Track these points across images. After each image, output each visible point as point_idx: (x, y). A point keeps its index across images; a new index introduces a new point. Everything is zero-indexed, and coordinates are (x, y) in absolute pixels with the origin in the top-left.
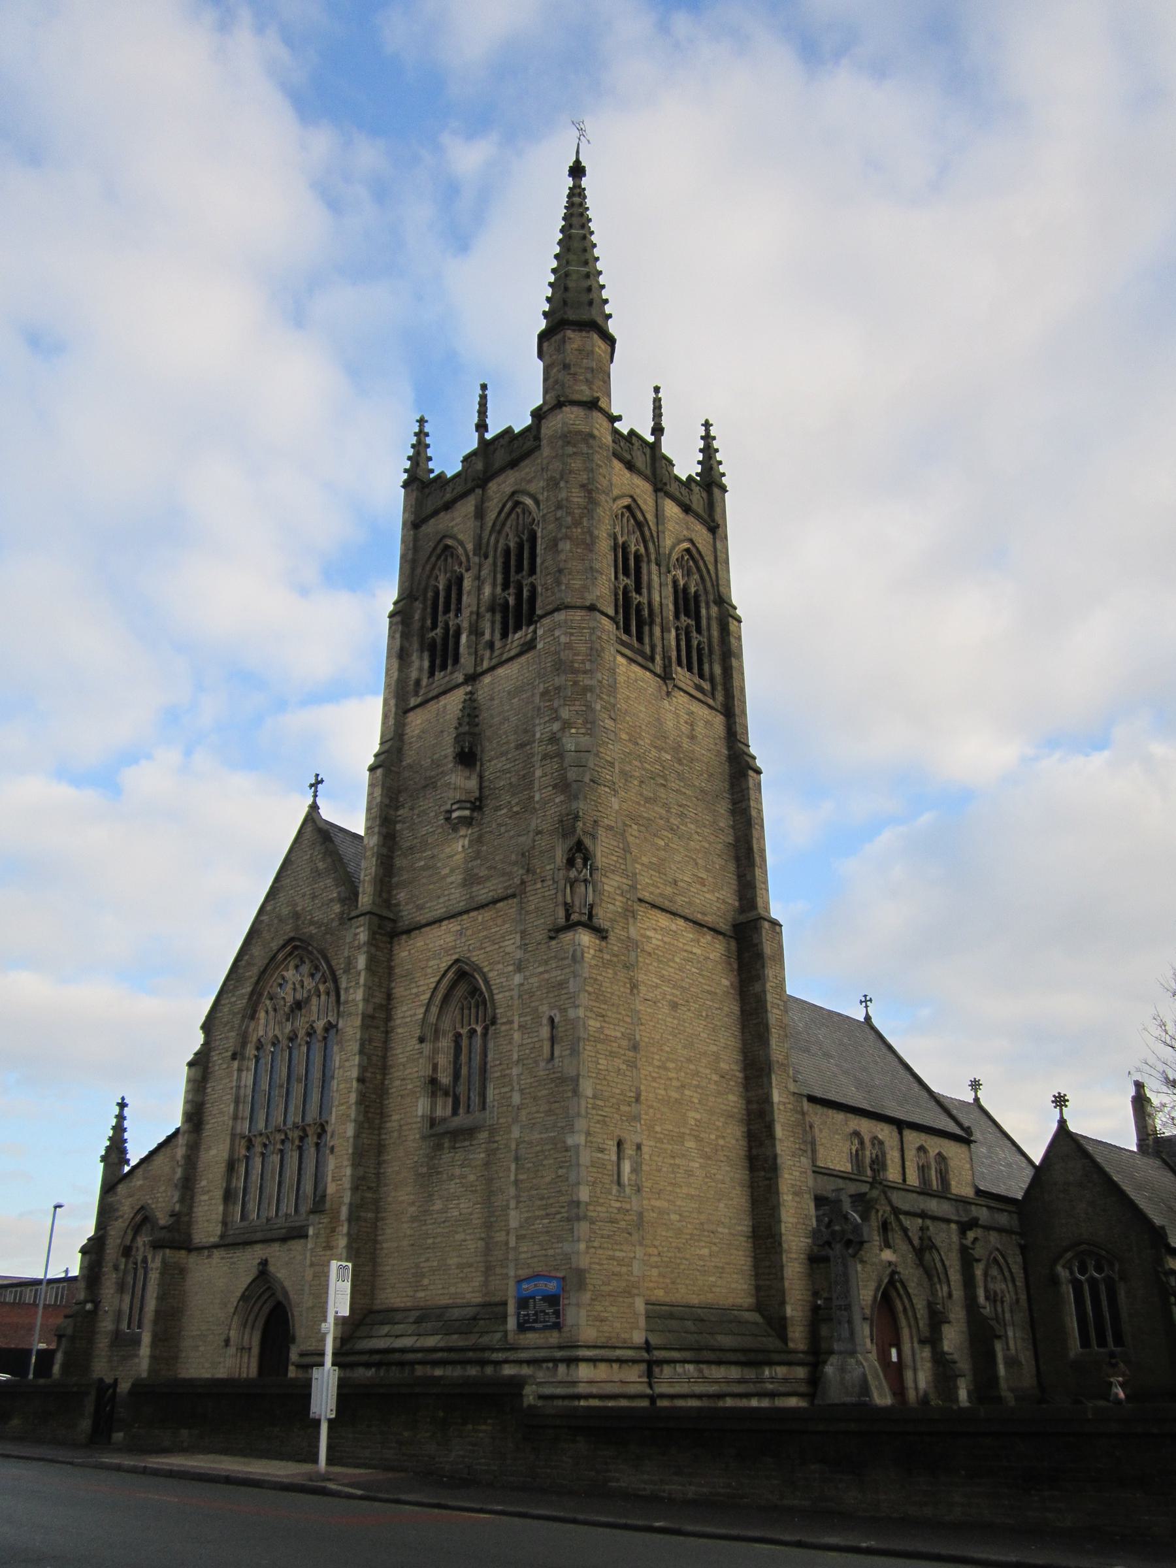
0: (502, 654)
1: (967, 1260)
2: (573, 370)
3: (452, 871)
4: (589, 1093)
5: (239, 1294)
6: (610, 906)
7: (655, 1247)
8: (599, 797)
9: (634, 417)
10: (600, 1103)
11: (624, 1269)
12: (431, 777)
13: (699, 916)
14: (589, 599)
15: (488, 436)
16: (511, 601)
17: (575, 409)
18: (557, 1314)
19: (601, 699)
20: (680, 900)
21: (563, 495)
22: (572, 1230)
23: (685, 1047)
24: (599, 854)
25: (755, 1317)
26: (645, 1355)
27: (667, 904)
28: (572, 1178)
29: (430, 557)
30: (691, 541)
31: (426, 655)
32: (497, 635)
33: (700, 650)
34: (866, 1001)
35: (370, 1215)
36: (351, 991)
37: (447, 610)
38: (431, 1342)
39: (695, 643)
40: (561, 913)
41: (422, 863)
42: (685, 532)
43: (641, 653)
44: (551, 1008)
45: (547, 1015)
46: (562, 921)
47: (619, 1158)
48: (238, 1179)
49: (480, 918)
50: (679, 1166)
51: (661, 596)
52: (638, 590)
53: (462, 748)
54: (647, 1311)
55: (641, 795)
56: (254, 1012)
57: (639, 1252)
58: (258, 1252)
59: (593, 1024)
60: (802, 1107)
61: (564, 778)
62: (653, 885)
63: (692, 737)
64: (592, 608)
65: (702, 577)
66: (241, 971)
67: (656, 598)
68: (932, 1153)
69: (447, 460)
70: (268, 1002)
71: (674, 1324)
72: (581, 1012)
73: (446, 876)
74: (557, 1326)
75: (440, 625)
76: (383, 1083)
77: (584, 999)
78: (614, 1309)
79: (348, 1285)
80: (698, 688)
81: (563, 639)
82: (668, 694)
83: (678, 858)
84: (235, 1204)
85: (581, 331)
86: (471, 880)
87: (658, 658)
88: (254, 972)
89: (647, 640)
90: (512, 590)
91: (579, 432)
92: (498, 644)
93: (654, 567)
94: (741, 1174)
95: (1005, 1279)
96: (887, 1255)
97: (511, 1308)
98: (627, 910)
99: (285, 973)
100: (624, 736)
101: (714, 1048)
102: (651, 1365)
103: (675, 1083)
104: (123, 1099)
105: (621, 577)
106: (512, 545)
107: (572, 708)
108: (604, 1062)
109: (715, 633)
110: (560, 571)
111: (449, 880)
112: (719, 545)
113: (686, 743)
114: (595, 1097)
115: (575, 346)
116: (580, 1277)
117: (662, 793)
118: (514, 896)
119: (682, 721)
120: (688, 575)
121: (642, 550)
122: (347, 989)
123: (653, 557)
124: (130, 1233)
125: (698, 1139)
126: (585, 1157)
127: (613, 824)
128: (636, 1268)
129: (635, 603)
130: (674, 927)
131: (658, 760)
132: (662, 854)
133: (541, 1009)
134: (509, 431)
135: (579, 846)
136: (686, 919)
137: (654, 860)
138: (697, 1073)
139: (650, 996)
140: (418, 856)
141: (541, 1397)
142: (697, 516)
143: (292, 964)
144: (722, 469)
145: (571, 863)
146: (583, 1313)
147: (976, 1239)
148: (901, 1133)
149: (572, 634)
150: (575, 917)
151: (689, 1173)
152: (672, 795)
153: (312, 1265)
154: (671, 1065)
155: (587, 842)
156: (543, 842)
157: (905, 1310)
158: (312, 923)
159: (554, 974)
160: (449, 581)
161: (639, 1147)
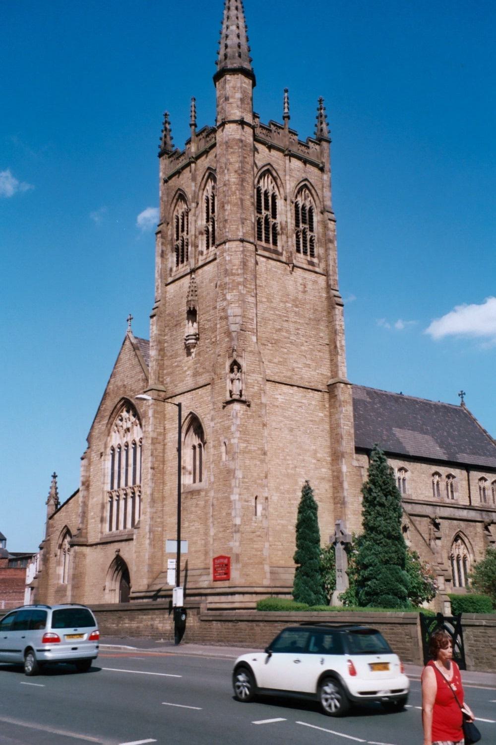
0: (206, 258)
2: (231, 100)
5: (109, 565)
6: (251, 389)
7: (280, 541)
8: (245, 337)
10: (246, 480)
11: (259, 553)
12: (178, 321)
13: (307, 383)
16: (211, 229)
19: (246, 287)
20: (295, 377)
21: (227, 178)
22: (233, 537)
29: (173, 200)
31: (175, 254)
34: (462, 394)
35: (160, 529)
36: (147, 426)
39: (308, 238)
40: (228, 394)
41: (176, 364)
45: (223, 441)
48: (107, 512)
49: (200, 393)
50: (293, 504)
51: (285, 216)
52: (274, 216)
53: (190, 308)
54: (270, 570)
55: (274, 328)
56: (109, 432)
58: (117, 546)
60: (361, 473)
61: (228, 329)
62: (280, 372)
63: (304, 292)
66: (102, 412)
70: (115, 427)
73: (186, 371)
76: (163, 468)
78: (254, 570)
80: (311, 263)
81: (228, 258)
84: (106, 523)
86: (196, 374)
87: (284, 253)
94: (332, 506)
98: (261, 390)
99: (122, 414)
100: (264, 300)
101: (314, 448)
103: (291, 466)
104: (55, 473)
105: (263, 211)
107: (232, 294)
108: (248, 462)
113: (300, 296)
114: (243, 478)
115: (231, 85)
117: (285, 324)
118: (209, 384)
119: (299, 284)
120: (305, 199)
122: (145, 426)
124: (61, 538)
126: (238, 505)
127: (253, 349)
129: (273, 223)
130: (291, 392)
131: (286, 309)
132: (286, 356)
133: (221, 438)
135: (235, 363)
136: (298, 387)
137: (281, 360)
138: (304, 460)
139: (278, 426)
140: (174, 360)
143: (125, 409)
145: (232, 371)
148: (468, 473)
149: (231, 255)
152: (291, 325)
153: (136, 552)
154: (288, 457)
155: (239, 360)
156: (220, 360)
158: (131, 390)
159: (226, 422)
160: (183, 213)
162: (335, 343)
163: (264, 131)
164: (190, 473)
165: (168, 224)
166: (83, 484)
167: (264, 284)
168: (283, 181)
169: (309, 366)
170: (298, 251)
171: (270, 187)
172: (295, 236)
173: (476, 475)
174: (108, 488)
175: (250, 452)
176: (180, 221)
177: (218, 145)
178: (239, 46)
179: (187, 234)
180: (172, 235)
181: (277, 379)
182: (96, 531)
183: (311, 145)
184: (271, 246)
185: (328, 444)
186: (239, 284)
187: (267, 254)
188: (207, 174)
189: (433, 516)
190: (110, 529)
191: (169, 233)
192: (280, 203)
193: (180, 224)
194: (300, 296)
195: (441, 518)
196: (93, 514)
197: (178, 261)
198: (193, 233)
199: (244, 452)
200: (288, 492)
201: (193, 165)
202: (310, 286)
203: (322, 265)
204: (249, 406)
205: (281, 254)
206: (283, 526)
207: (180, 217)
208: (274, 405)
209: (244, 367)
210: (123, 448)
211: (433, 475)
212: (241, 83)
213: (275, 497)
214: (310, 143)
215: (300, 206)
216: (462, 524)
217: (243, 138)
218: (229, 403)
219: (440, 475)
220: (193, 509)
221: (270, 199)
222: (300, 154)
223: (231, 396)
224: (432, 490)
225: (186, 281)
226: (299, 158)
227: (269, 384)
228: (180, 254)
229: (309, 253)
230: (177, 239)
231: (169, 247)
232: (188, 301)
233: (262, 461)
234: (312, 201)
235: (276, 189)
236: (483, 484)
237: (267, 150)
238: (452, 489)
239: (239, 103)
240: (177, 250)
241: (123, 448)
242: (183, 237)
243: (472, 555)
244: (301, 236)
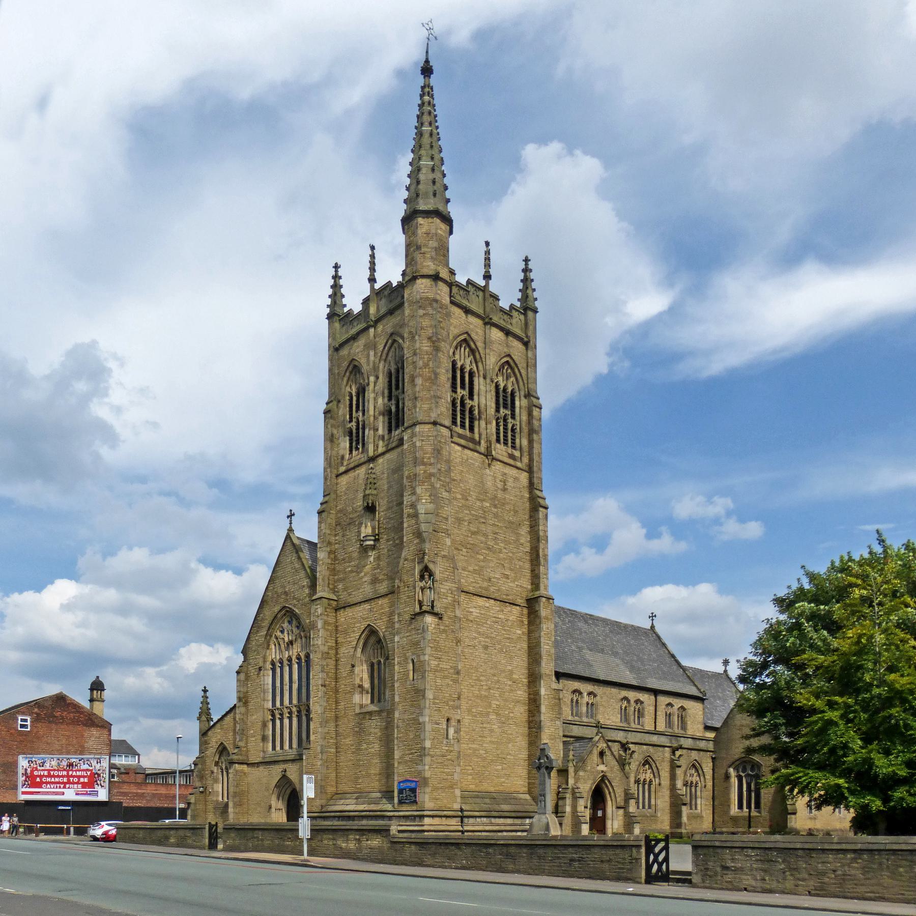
1: (674, 767)
2: (423, 250)
3: (365, 575)
4: (431, 697)
9: (467, 271)
14: (433, 416)
15: (377, 286)
17: (424, 280)
18: (415, 796)
19: (440, 480)
20: (492, 589)
23: (492, 668)
24: (437, 572)
25: (528, 797)
26: (460, 813)
27: (484, 593)
28: (422, 737)
30: (509, 356)
31: (348, 438)
32: (386, 432)
33: (513, 430)
37: (357, 411)
38: (361, 807)
39: (510, 426)
40: (417, 606)
42: (506, 350)
43: (472, 440)
44: (413, 654)
46: (417, 610)
47: (447, 726)
51: (485, 398)
52: (471, 396)
56: (269, 645)
57: (458, 769)
58: (283, 766)
59: (434, 663)
61: (418, 529)
64: (435, 423)
65: (517, 379)
67: (483, 401)
68: (676, 707)
69: (353, 302)
71: (478, 800)
72: (427, 657)
74: (415, 802)
75: (354, 420)
77: (428, 651)
79: (313, 785)
80: (512, 456)
81: (418, 444)
82: (489, 465)
83: (492, 564)
85: (428, 217)
86: (375, 581)
87: (483, 442)
88: (266, 624)
89: (476, 430)
90: (393, 402)
91: (427, 298)
92: (386, 437)
93: (481, 379)
94: (525, 730)
95: (699, 775)
96: (602, 768)
97: (396, 794)
100: (459, 496)
101: (510, 668)
102: (462, 817)
103: (485, 687)
105: (459, 390)
106: (393, 371)
109: (525, 418)
110: (416, 398)
111: (364, 580)
112: (530, 354)
113: (500, 494)
114: (434, 699)
115: (424, 230)
116: (425, 782)
120: (507, 379)
121: (475, 369)
123: (481, 373)
125: (498, 714)
126: (428, 727)
128: (456, 777)
130: (487, 605)
131: (482, 508)
132: (482, 564)
134: (389, 283)
135: (426, 568)
136: (495, 600)
137: (476, 568)
138: (498, 681)
141: (399, 831)
142: (516, 337)
144: (535, 295)
145: (422, 578)
146: (427, 796)
147: (680, 755)
148: (656, 697)
149: (423, 441)
150: (424, 608)
151: (492, 731)
154: (482, 678)
155: (431, 566)
157: (610, 793)
158: (294, 598)
161: (459, 721)
162: (538, 552)
163: (461, 292)
164: (367, 693)
165: (339, 401)
166: (240, 699)
167: (458, 477)
168: (483, 356)
169: (507, 577)
170: (498, 441)
171: (468, 361)
172: (494, 422)
173: (663, 700)
174: (270, 705)
175: (442, 670)
176: (355, 398)
177: (406, 304)
178: (434, 182)
179: (364, 414)
180: (345, 416)
181: (471, 589)
182: (256, 750)
183: (515, 314)
184: (468, 433)
185: (526, 665)
186: (432, 475)
187: (463, 442)
188: (390, 341)
189: (624, 741)
190: (274, 748)
191: (340, 413)
192: (479, 383)
193: (354, 402)
194: (500, 494)
195: (632, 743)
196: (254, 731)
197: (351, 447)
198: (371, 412)
199: (436, 671)
200: (481, 714)
201: (372, 330)
202: (510, 483)
203: (526, 460)
204: (441, 618)
205: (479, 443)
206: (475, 750)
207: (354, 394)
208: (468, 620)
209: (438, 575)
210: (286, 662)
211: (622, 700)
212: (437, 229)
213: (467, 720)
214: (514, 311)
215: (502, 387)
216: (651, 749)
217: (438, 297)
218: (416, 615)
219: (580, 693)
220: (372, 730)
221: (467, 375)
222: (502, 323)
223: (421, 608)
224: (619, 716)
225: (362, 471)
226: (502, 329)
227: (463, 596)
228: (354, 439)
229: (510, 444)
230: (351, 421)
231: (341, 430)
232: (364, 496)
233: (456, 681)
234: (515, 382)
235: (474, 365)
236: (670, 710)
237: (463, 315)
238: (640, 714)
239: (433, 254)
240: (350, 433)
241: (286, 662)
242: (358, 419)
243: (657, 780)
244: (502, 424)
